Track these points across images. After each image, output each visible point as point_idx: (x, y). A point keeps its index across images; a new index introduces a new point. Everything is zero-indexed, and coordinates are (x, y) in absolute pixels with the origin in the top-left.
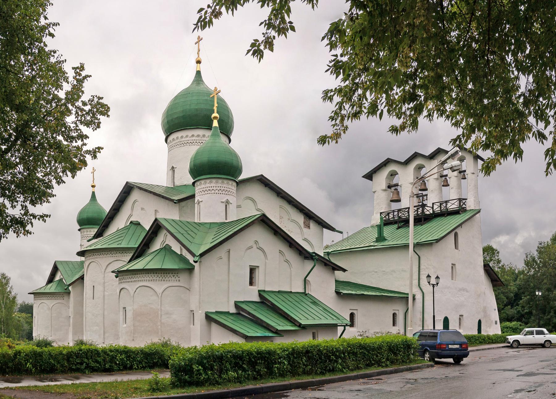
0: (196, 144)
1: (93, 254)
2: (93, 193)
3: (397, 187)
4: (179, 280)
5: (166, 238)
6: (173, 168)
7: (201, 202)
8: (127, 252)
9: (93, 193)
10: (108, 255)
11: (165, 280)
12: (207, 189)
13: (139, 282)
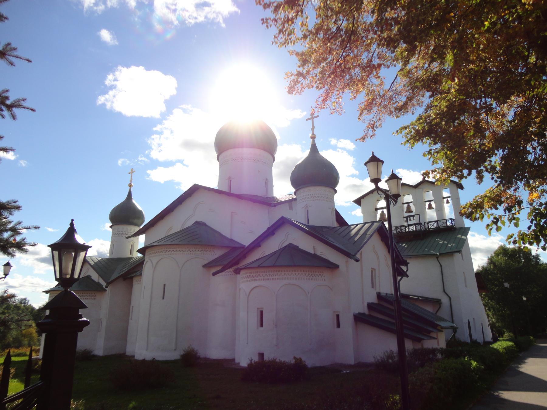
1: (166, 249)
7: (310, 206)
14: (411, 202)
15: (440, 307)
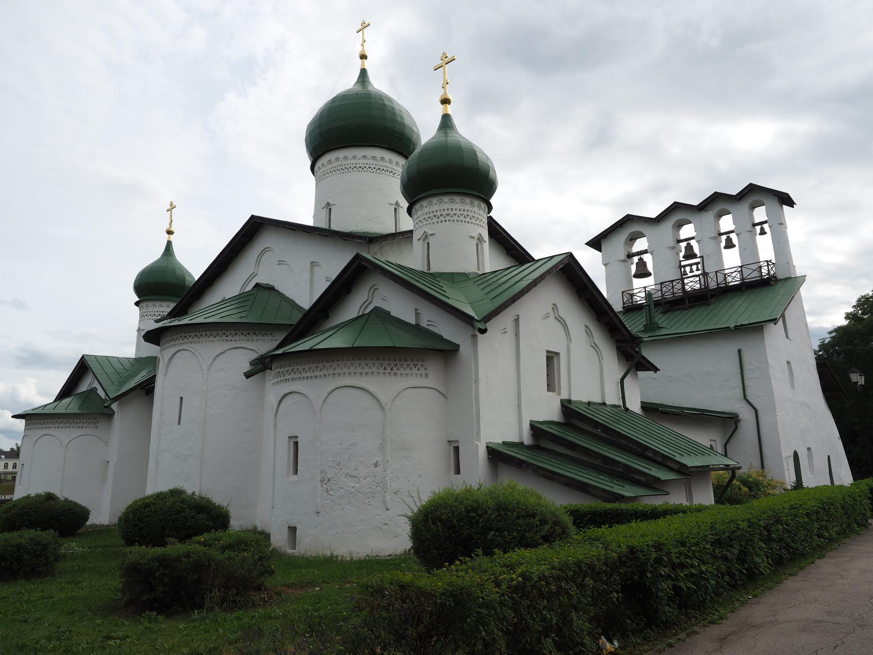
0: (370, 170)
1: (184, 335)
2: (169, 243)
3: (642, 256)
4: (426, 375)
5: (372, 297)
6: (328, 204)
7: (431, 235)
8: (257, 333)
9: (169, 243)
10: (218, 338)
11: (399, 374)
12: (444, 213)
13: (43, 430)
14: (693, 238)
15: (736, 428)
